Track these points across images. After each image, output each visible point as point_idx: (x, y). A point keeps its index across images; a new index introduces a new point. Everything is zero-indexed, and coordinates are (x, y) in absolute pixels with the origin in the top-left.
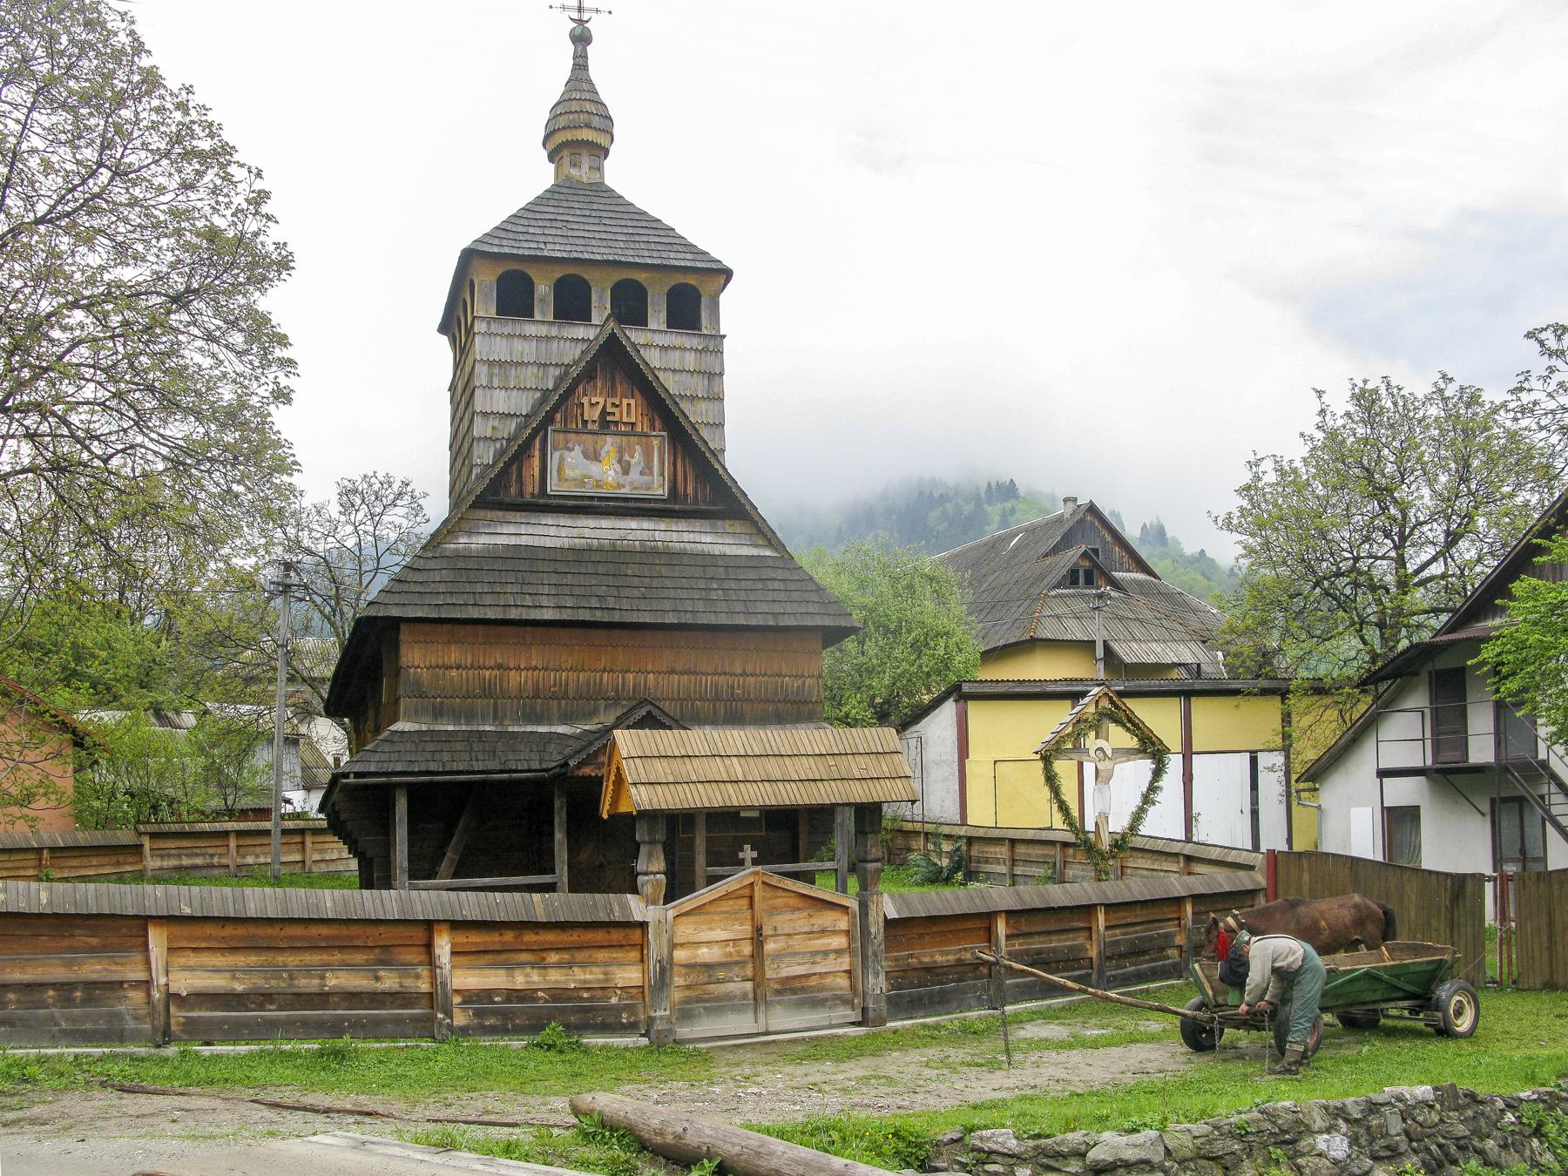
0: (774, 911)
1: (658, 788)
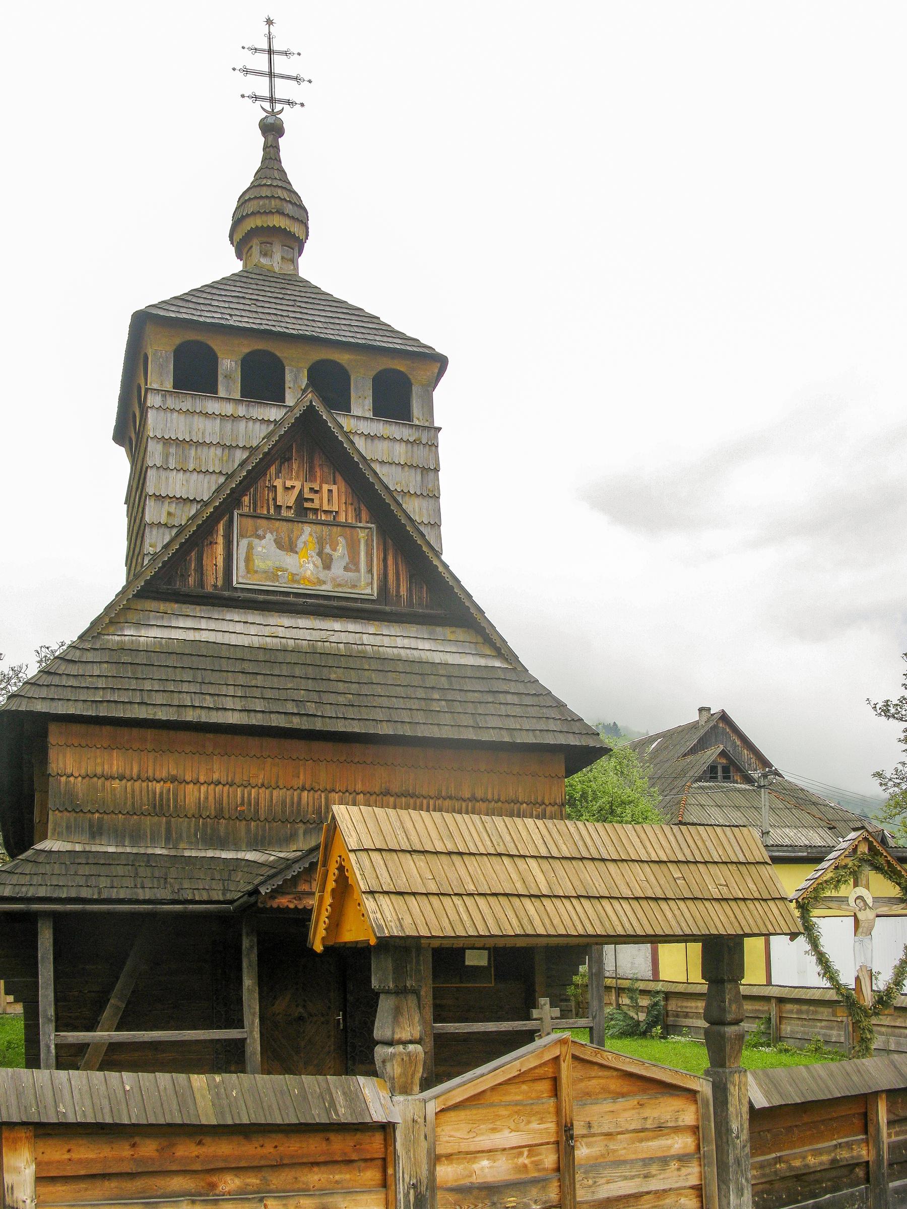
0: (587, 1097)
1: (411, 900)
